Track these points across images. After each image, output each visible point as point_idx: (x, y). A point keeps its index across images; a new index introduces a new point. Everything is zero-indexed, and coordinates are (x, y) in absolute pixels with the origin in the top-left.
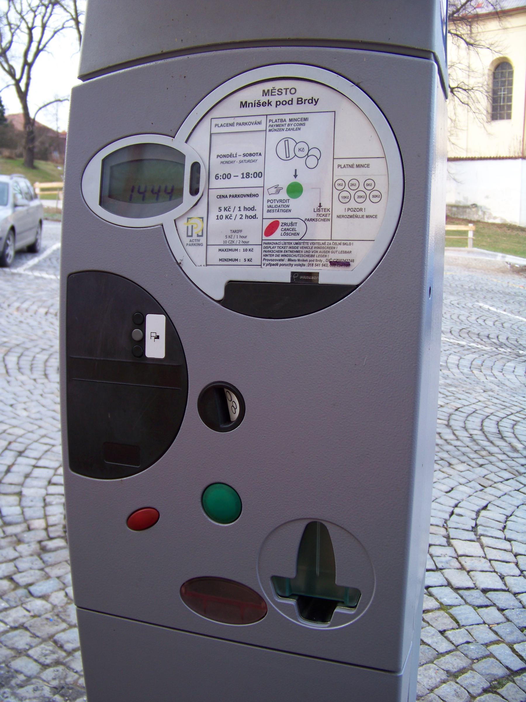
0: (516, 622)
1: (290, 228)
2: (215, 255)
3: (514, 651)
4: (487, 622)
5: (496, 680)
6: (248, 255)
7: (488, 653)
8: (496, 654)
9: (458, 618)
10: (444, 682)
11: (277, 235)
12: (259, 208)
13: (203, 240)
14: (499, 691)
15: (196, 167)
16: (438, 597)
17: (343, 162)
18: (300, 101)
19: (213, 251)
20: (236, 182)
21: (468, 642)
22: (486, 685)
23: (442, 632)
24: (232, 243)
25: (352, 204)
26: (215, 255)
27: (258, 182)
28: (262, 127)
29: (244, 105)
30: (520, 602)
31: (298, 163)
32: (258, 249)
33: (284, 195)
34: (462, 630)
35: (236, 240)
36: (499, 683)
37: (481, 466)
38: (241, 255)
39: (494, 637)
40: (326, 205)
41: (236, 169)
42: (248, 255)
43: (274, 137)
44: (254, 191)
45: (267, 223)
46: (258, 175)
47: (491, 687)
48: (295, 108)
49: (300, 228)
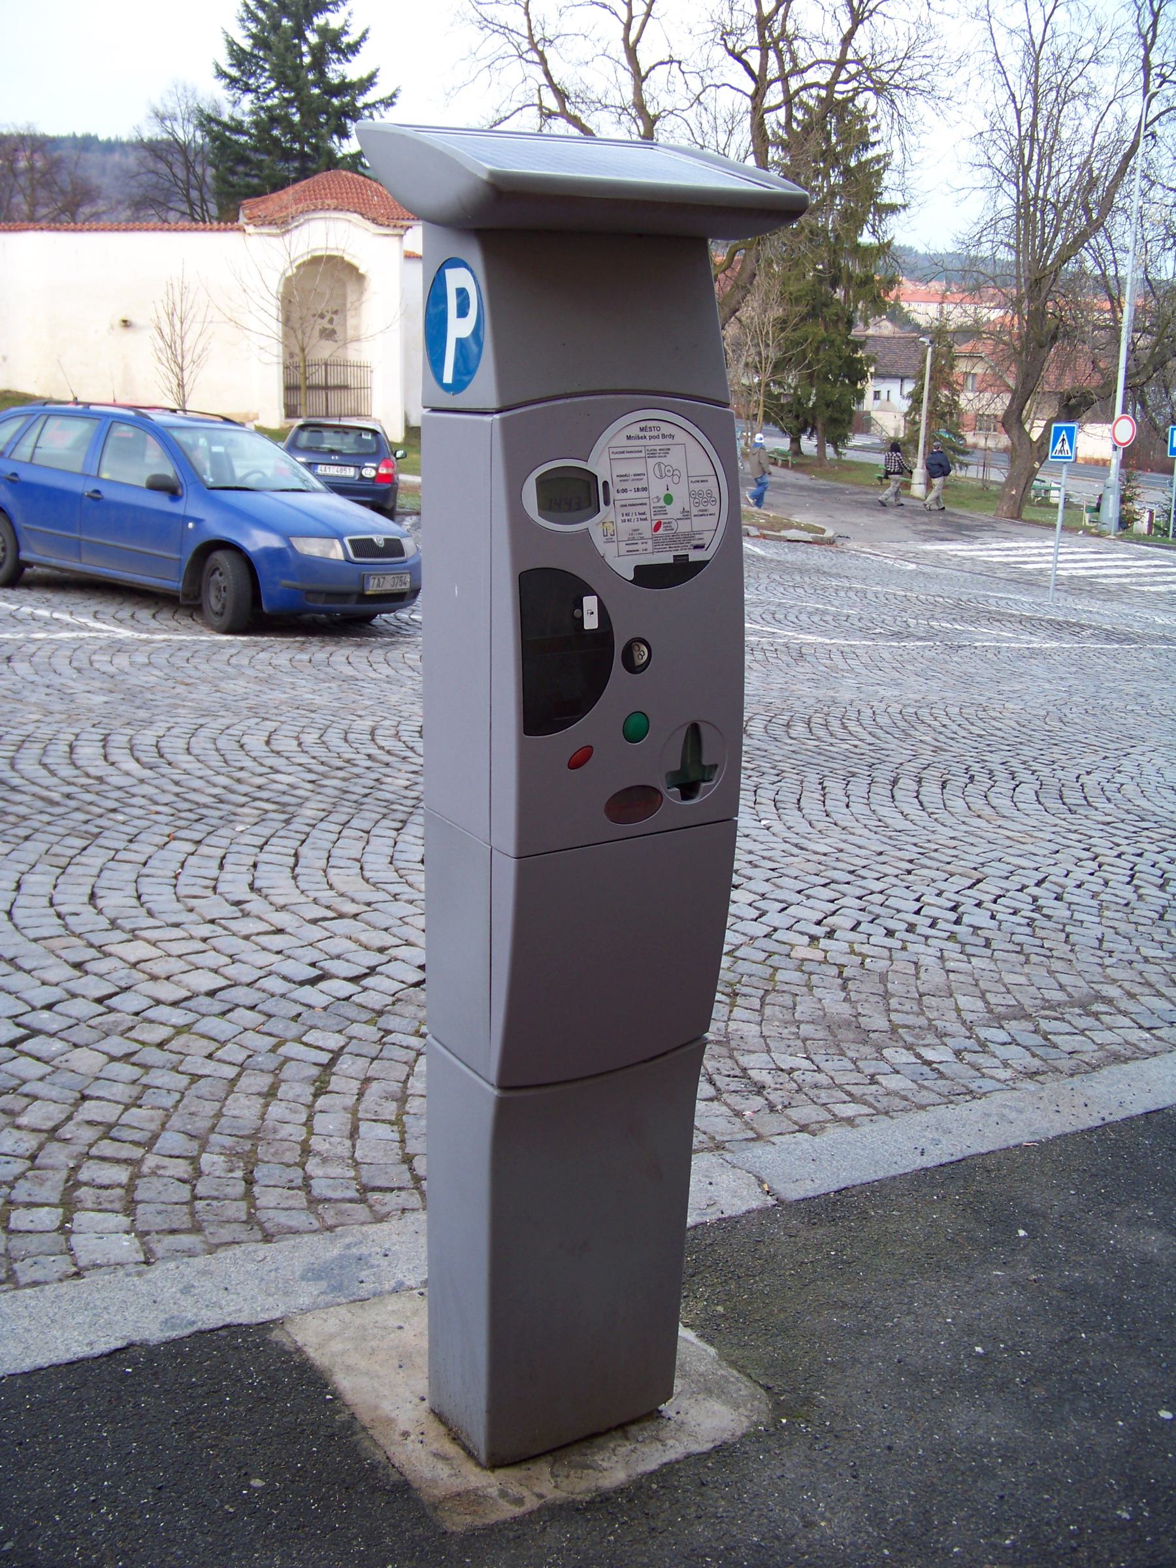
0: (282, 1013)
1: (668, 527)
2: (624, 548)
3: (306, 1044)
4: (248, 1026)
5: (315, 1081)
6: (644, 546)
7: (282, 1058)
8: (291, 1055)
9: (212, 1034)
10: (267, 1105)
11: (661, 531)
12: (648, 512)
13: (615, 538)
14: (329, 1089)
15: (605, 484)
16: (163, 1019)
17: (694, 479)
18: (664, 436)
19: (622, 545)
20: (631, 495)
21: (250, 1056)
22: (312, 1090)
23: (210, 1056)
24: (633, 539)
25: (701, 507)
26: (624, 548)
27: (645, 494)
28: (643, 455)
29: (629, 438)
30: (264, 991)
31: (668, 480)
32: (650, 542)
33: (662, 503)
34: (229, 1045)
35: (636, 537)
36: (322, 1082)
37: (27, 838)
38: (640, 547)
39: (273, 1041)
40: (687, 509)
41: (629, 485)
42: (644, 546)
43: (652, 462)
44: (644, 501)
45: (654, 523)
46: (645, 489)
47: (317, 1089)
48: (661, 441)
49: (674, 525)
